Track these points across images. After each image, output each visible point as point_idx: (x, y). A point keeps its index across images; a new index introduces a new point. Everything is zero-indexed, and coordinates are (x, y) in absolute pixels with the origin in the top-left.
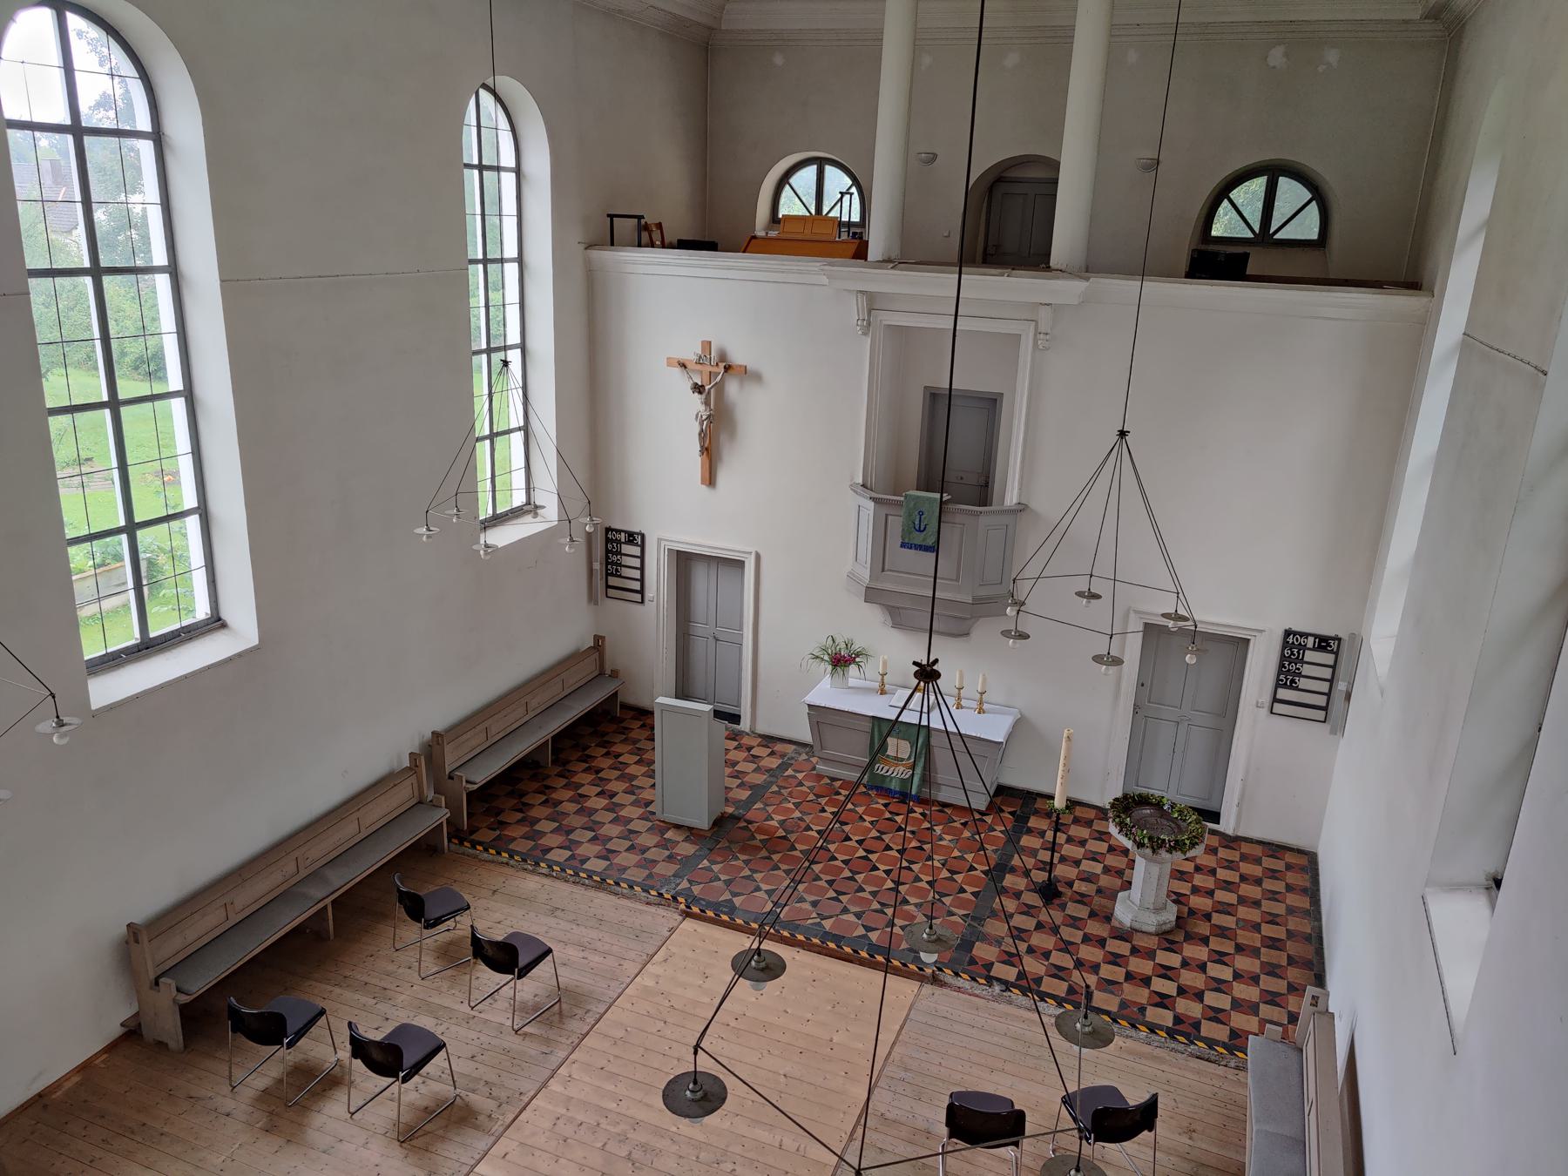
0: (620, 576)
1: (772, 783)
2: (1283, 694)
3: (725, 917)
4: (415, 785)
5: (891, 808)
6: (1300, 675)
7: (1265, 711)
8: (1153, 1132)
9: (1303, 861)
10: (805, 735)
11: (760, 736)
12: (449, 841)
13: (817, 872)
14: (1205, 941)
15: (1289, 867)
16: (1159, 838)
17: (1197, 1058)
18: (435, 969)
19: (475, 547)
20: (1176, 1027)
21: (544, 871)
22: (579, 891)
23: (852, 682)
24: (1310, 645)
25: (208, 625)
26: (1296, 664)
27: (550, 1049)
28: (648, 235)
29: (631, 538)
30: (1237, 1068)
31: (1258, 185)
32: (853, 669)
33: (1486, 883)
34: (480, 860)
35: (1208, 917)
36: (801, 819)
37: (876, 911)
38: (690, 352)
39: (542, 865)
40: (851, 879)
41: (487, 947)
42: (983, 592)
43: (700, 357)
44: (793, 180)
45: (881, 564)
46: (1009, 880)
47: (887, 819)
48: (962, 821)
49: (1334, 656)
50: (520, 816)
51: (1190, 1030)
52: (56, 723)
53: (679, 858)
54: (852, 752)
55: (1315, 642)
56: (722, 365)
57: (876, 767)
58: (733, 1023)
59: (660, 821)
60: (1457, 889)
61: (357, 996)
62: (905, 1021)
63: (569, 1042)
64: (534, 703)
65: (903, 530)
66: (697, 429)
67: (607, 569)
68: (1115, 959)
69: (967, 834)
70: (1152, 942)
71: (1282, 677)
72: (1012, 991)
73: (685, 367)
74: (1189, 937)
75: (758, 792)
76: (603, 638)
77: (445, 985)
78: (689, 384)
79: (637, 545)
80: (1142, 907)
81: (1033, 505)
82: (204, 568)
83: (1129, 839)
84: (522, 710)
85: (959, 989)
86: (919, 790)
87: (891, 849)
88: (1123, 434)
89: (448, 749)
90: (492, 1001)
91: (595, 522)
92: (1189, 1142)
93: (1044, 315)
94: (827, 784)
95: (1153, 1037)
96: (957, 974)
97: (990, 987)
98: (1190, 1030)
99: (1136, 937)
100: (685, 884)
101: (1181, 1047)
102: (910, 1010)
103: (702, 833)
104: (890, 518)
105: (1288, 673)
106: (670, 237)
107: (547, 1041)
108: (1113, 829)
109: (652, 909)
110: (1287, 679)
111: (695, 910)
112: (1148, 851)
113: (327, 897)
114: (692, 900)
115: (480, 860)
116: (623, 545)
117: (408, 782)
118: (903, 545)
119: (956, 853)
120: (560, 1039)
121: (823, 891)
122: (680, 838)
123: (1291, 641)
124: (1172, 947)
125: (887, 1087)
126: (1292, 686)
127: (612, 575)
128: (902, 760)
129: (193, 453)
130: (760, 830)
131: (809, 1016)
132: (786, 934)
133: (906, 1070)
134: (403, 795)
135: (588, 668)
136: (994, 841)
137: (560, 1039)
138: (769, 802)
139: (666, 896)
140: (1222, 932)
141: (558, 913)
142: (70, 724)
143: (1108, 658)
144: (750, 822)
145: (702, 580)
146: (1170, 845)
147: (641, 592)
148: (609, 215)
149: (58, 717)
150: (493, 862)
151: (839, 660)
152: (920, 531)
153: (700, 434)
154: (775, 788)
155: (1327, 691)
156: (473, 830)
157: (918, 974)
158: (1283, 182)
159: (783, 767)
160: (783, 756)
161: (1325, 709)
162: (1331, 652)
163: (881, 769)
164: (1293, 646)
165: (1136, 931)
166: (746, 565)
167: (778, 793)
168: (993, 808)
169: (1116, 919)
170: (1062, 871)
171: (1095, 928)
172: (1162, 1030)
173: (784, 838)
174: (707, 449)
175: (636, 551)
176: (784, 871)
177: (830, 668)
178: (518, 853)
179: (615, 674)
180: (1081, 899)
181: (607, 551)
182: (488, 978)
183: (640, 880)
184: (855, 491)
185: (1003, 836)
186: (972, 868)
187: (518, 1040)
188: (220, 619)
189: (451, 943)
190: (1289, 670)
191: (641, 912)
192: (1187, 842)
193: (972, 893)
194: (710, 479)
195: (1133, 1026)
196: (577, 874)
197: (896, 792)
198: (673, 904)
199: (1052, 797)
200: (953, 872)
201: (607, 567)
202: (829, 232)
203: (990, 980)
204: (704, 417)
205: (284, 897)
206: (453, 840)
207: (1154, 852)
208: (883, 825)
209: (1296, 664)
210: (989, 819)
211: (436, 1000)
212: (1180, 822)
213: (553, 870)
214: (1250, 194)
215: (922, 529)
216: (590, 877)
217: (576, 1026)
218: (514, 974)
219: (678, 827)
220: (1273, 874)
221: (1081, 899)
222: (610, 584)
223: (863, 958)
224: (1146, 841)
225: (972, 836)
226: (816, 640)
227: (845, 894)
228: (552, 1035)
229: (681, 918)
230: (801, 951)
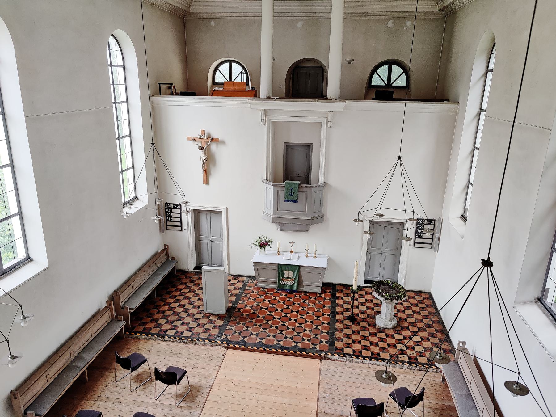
0: (172, 221)
1: (242, 293)
2: (417, 240)
3: (243, 347)
4: (110, 314)
5: (288, 296)
6: (172, 217)
7: (412, 246)
8: (423, 401)
9: (428, 296)
10: (253, 274)
11: (232, 275)
12: (125, 333)
13: (270, 324)
14: (408, 329)
15: (424, 298)
16: (393, 296)
17: (419, 370)
18: (135, 387)
19: (122, 214)
20: (410, 361)
21: (167, 339)
22: (183, 345)
23: (267, 252)
24: (426, 223)
25: (25, 261)
26: (421, 230)
27: (193, 411)
28: (172, 91)
29: (176, 206)
30: (433, 372)
31: (386, 67)
32: (267, 246)
33: (535, 300)
34: (139, 339)
35: (406, 320)
36: (257, 305)
37: (296, 335)
38: (197, 135)
39: (166, 337)
40: (284, 325)
41: (162, 374)
42: (315, 215)
43: (201, 136)
44: (220, 68)
45: (277, 208)
46: (338, 317)
47: (288, 301)
48: (314, 297)
49: (433, 226)
50: (150, 319)
51: (415, 361)
52: (23, 318)
53: (218, 326)
54: (272, 276)
55: (427, 222)
56: (210, 139)
57: (281, 282)
58: (259, 387)
59: (206, 313)
60: (525, 304)
61: (106, 404)
62: (320, 376)
63: (200, 407)
64: (147, 274)
65: (285, 195)
66: (202, 163)
67: (166, 219)
68: (382, 340)
69: (317, 302)
70: (392, 332)
71: (417, 235)
72: (353, 358)
73: (195, 140)
74: (403, 328)
75: (238, 296)
76: (167, 245)
77: (142, 393)
78: (197, 147)
79: (178, 209)
80: (386, 320)
81: (329, 183)
82: (22, 238)
83: (383, 297)
84: (143, 278)
85: (334, 360)
86: (297, 289)
87: (293, 311)
88: (400, 158)
89: (121, 296)
90: (163, 396)
91: (160, 200)
92: (428, 401)
93: (330, 115)
94: (262, 290)
95: (404, 366)
96: (333, 355)
97: (345, 357)
98: (415, 361)
99: (386, 330)
100: (224, 337)
101: (413, 368)
102: (320, 371)
103: (223, 316)
104: (279, 191)
105: (419, 233)
106: (178, 91)
107: (191, 408)
108: (375, 294)
109: (214, 348)
110: (419, 235)
111: (231, 346)
112: (389, 301)
113: (85, 366)
114: (229, 342)
115: (139, 339)
116: (172, 209)
117: (107, 313)
118: (285, 201)
119: (316, 310)
120: (196, 406)
121: (292, 333)
122: (216, 319)
123: (419, 222)
124: (399, 333)
125: (323, 401)
126: (420, 237)
127: (169, 221)
128: (290, 278)
129: (15, 190)
130: (244, 311)
131: (285, 379)
132: (268, 349)
133: (327, 393)
134: (105, 319)
135: (163, 257)
136: (327, 303)
137: (196, 406)
138: (244, 300)
139: (218, 342)
140: (412, 324)
141: (178, 355)
142: (28, 317)
143: (406, 238)
144: (240, 309)
145: (204, 220)
146: (397, 297)
147: (181, 226)
148: (158, 84)
149: (23, 315)
150: (144, 339)
151: (263, 245)
152: (291, 195)
153: (203, 165)
154: (244, 295)
155: (432, 238)
156: (133, 327)
157: (319, 357)
158: (394, 67)
159: (245, 286)
160: (243, 282)
161: (431, 244)
162: (433, 225)
163: (282, 283)
164: (420, 224)
165: (385, 328)
166: (223, 212)
167: (246, 296)
168: (323, 291)
169: (378, 325)
170: (356, 311)
171: (371, 330)
172: (406, 363)
173: (254, 313)
174: (205, 171)
175: (178, 211)
176: (258, 325)
177: (259, 248)
178: (155, 334)
179: (173, 259)
180: (364, 320)
181: (166, 212)
182: (160, 385)
183: (206, 337)
184: (264, 182)
185: (329, 301)
186: (324, 315)
187: (179, 409)
188: (29, 258)
189: (138, 375)
190: (419, 232)
191: (210, 350)
192: (402, 296)
193: (327, 324)
194: (207, 182)
195: (397, 363)
196: (181, 339)
197: (288, 290)
198: (221, 345)
199: (352, 286)
200: (318, 317)
201: (166, 218)
202: (235, 88)
203: (345, 355)
204: (204, 159)
205: (68, 368)
206: (127, 333)
207: (392, 301)
208: (288, 303)
209: (421, 230)
210: (323, 295)
211: (140, 399)
212: (396, 289)
213: (171, 339)
214: (383, 71)
215: (292, 194)
216: (186, 339)
217: (199, 399)
218: (175, 384)
219: (213, 315)
220: (420, 302)
221: (364, 320)
222: (168, 224)
223: (298, 354)
224: (389, 297)
225: (319, 303)
226: (254, 238)
227: (284, 331)
228: (192, 404)
229: (226, 349)
230: (274, 355)
